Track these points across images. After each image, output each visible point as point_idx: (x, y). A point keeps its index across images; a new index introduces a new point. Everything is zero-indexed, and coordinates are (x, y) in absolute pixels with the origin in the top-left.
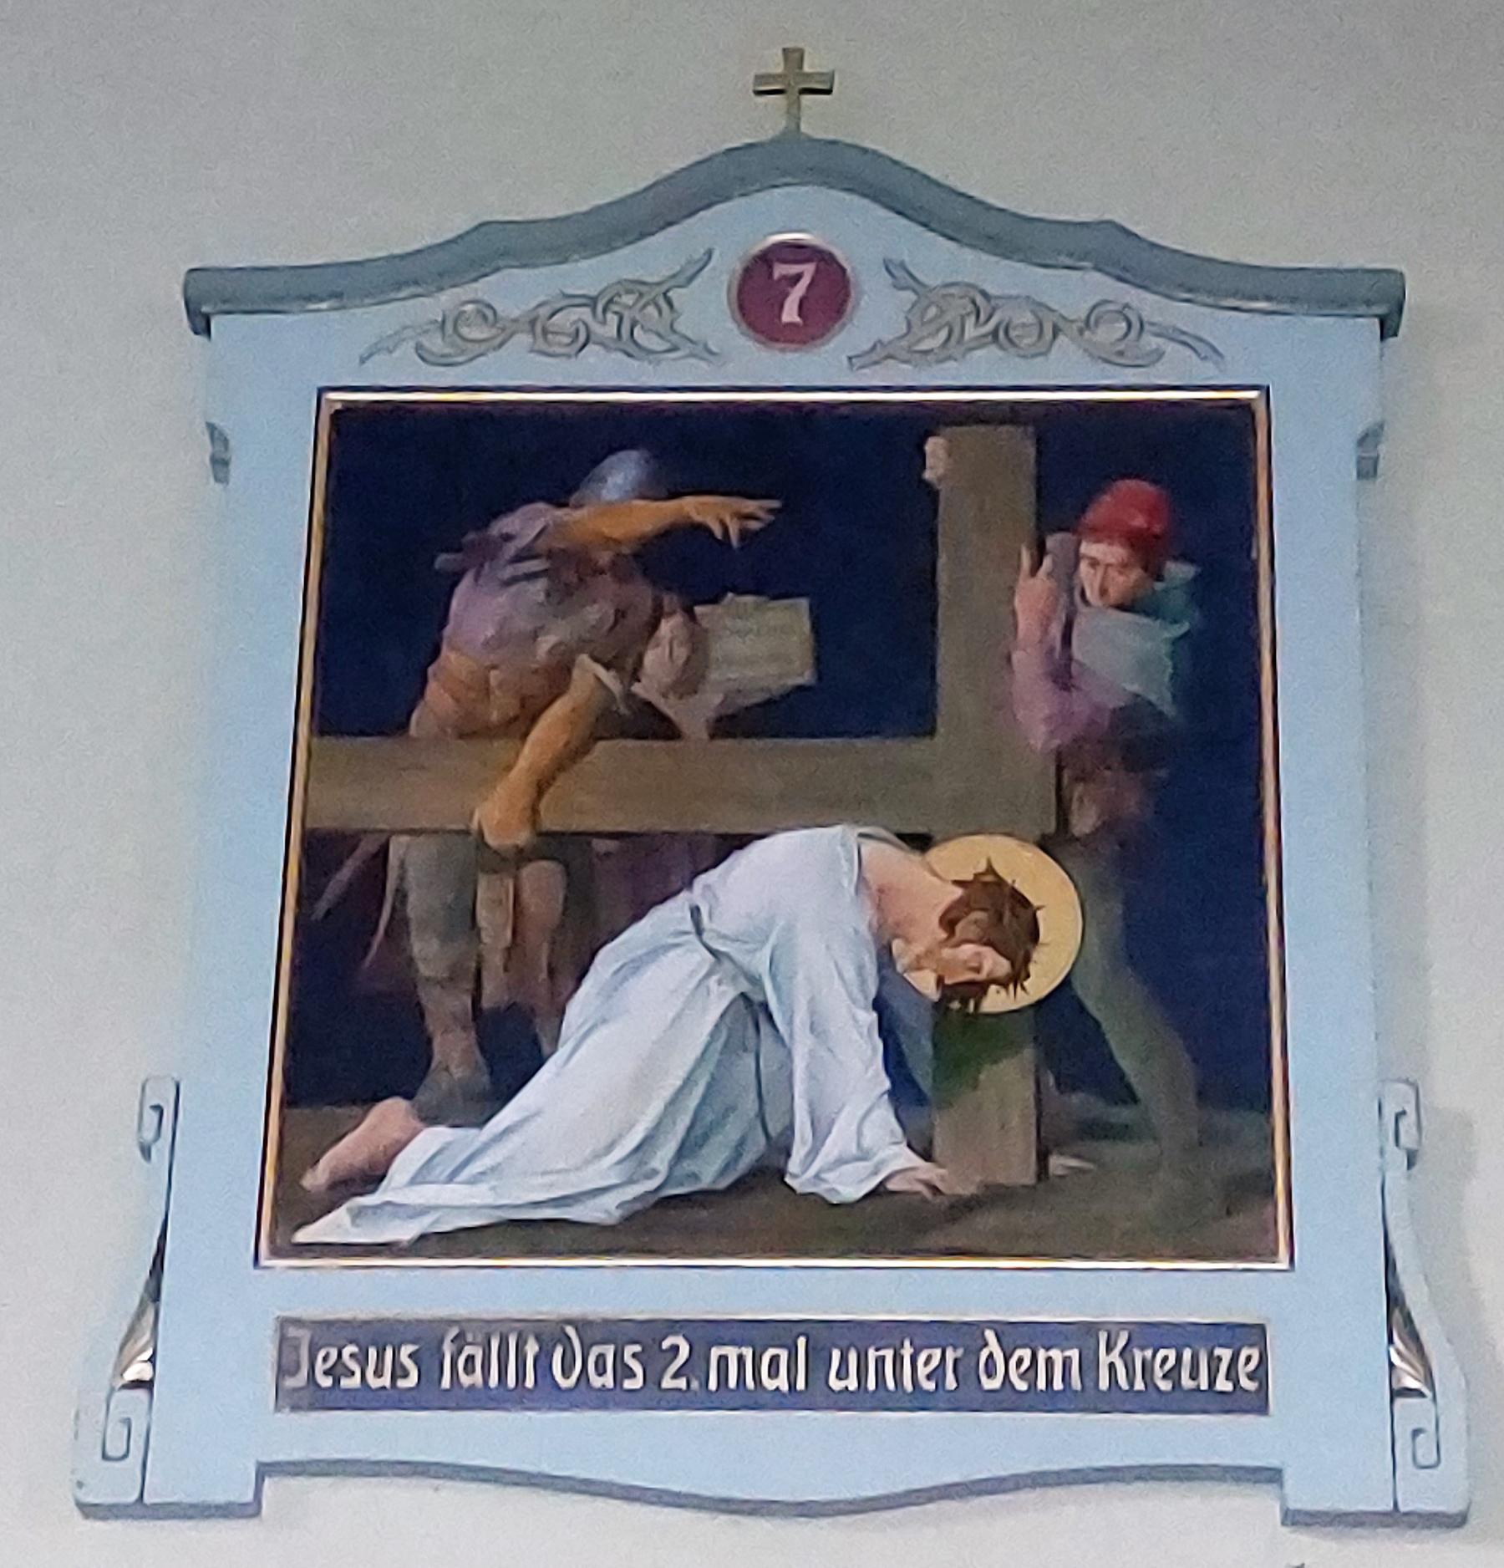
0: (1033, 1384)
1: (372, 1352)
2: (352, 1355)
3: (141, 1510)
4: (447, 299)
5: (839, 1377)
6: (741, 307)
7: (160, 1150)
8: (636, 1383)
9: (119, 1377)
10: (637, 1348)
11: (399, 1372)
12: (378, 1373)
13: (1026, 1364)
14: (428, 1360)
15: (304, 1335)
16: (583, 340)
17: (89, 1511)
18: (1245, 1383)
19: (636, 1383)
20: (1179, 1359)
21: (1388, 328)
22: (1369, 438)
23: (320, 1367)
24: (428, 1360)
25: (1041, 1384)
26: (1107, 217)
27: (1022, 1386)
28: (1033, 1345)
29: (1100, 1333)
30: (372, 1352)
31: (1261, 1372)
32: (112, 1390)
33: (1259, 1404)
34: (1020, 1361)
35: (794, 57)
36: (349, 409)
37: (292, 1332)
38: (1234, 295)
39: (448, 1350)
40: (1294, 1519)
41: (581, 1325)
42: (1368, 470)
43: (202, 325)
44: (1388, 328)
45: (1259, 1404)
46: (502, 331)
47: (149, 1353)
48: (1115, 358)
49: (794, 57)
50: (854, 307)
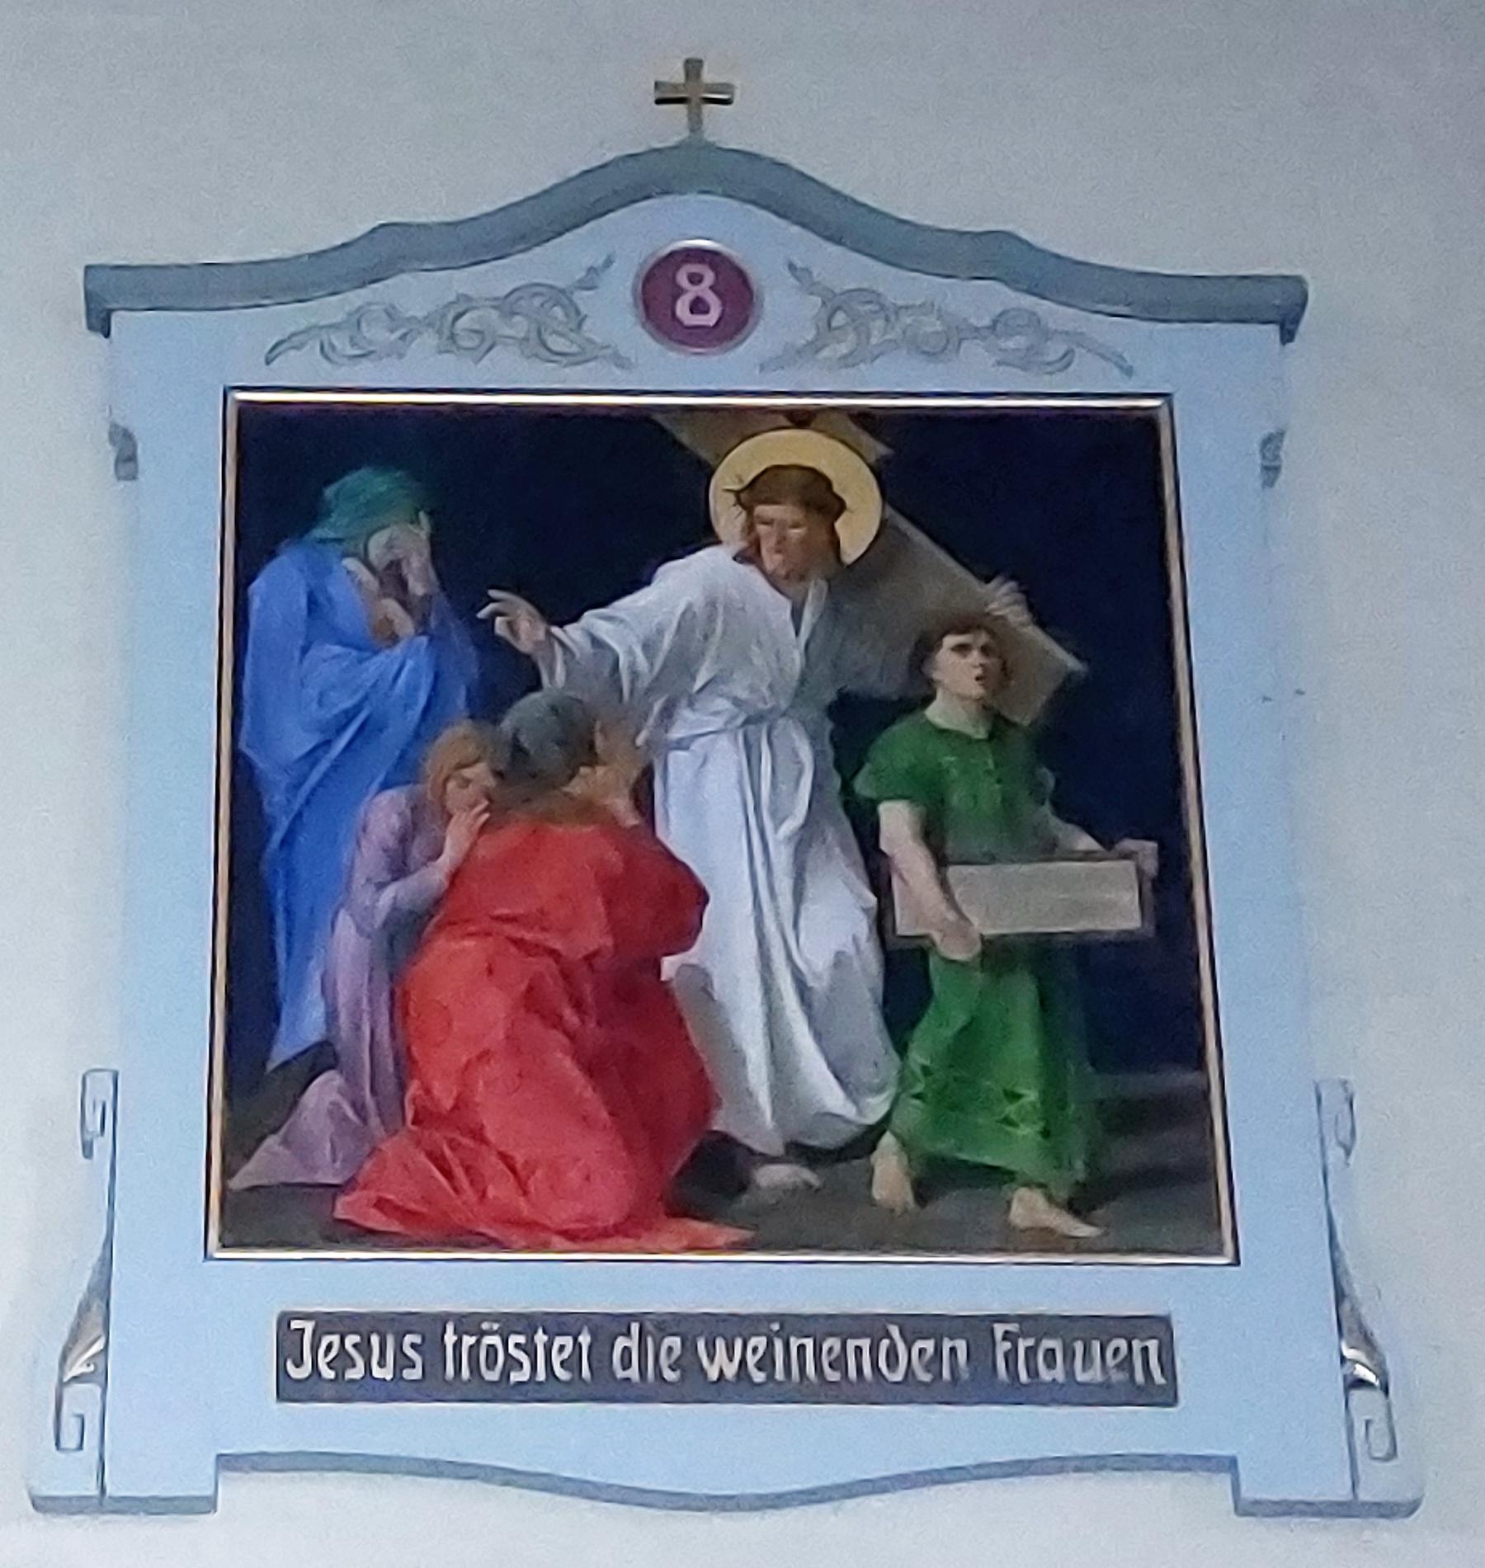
0: (771, 1377)
1: (375, 1340)
2: (355, 1346)
3: (102, 1504)
4: (356, 298)
5: (1085, 1369)
6: (647, 307)
7: (102, 1145)
8: (415, 1374)
9: (85, 1365)
10: (417, 1339)
11: (402, 1362)
12: (382, 1364)
13: (677, 1352)
14: (432, 1348)
15: (309, 1326)
16: (486, 342)
17: (43, 1505)
18: (560, 1372)
19: (415, 1374)
20: (577, 1346)
21: (1287, 336)
22: (1272, 443)
23: (664, 1361)
24: (432, 1348)
25: (852, 1372)
26: (1009, 228)
27: (926, 1377)
28: (382, 1330)
29: (1017, 1325)
30: (375, 1340)
31: (768, 1361)
32: (62, 1385)
33: (1167, 1396)
34: (1117, 1351)
35: (693, 67)
36: (245, 408)
37: (295, 1324)
38: (1104, 301)
39: (450, 1338)
40: (1245, 1508)
41: (902, 1320)
42: (1271, 471)
43: (100, 322)
44: (1287, 336)
45: (1167, 1396)
46: (406, 329)
47: (98, 1346)
48: (1027, 360)
49: (693, 67)
50: (636, 290)
